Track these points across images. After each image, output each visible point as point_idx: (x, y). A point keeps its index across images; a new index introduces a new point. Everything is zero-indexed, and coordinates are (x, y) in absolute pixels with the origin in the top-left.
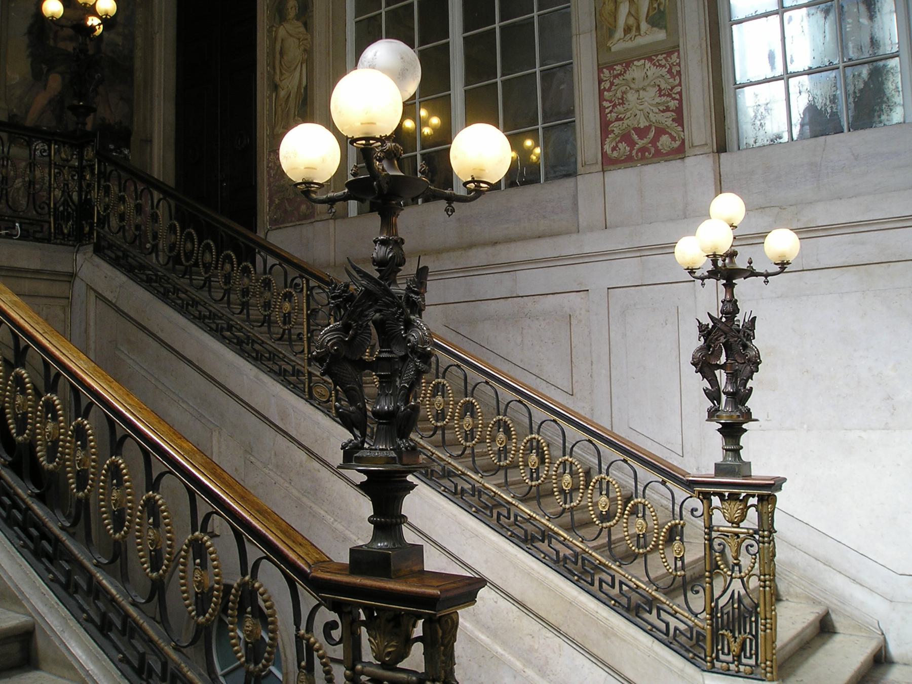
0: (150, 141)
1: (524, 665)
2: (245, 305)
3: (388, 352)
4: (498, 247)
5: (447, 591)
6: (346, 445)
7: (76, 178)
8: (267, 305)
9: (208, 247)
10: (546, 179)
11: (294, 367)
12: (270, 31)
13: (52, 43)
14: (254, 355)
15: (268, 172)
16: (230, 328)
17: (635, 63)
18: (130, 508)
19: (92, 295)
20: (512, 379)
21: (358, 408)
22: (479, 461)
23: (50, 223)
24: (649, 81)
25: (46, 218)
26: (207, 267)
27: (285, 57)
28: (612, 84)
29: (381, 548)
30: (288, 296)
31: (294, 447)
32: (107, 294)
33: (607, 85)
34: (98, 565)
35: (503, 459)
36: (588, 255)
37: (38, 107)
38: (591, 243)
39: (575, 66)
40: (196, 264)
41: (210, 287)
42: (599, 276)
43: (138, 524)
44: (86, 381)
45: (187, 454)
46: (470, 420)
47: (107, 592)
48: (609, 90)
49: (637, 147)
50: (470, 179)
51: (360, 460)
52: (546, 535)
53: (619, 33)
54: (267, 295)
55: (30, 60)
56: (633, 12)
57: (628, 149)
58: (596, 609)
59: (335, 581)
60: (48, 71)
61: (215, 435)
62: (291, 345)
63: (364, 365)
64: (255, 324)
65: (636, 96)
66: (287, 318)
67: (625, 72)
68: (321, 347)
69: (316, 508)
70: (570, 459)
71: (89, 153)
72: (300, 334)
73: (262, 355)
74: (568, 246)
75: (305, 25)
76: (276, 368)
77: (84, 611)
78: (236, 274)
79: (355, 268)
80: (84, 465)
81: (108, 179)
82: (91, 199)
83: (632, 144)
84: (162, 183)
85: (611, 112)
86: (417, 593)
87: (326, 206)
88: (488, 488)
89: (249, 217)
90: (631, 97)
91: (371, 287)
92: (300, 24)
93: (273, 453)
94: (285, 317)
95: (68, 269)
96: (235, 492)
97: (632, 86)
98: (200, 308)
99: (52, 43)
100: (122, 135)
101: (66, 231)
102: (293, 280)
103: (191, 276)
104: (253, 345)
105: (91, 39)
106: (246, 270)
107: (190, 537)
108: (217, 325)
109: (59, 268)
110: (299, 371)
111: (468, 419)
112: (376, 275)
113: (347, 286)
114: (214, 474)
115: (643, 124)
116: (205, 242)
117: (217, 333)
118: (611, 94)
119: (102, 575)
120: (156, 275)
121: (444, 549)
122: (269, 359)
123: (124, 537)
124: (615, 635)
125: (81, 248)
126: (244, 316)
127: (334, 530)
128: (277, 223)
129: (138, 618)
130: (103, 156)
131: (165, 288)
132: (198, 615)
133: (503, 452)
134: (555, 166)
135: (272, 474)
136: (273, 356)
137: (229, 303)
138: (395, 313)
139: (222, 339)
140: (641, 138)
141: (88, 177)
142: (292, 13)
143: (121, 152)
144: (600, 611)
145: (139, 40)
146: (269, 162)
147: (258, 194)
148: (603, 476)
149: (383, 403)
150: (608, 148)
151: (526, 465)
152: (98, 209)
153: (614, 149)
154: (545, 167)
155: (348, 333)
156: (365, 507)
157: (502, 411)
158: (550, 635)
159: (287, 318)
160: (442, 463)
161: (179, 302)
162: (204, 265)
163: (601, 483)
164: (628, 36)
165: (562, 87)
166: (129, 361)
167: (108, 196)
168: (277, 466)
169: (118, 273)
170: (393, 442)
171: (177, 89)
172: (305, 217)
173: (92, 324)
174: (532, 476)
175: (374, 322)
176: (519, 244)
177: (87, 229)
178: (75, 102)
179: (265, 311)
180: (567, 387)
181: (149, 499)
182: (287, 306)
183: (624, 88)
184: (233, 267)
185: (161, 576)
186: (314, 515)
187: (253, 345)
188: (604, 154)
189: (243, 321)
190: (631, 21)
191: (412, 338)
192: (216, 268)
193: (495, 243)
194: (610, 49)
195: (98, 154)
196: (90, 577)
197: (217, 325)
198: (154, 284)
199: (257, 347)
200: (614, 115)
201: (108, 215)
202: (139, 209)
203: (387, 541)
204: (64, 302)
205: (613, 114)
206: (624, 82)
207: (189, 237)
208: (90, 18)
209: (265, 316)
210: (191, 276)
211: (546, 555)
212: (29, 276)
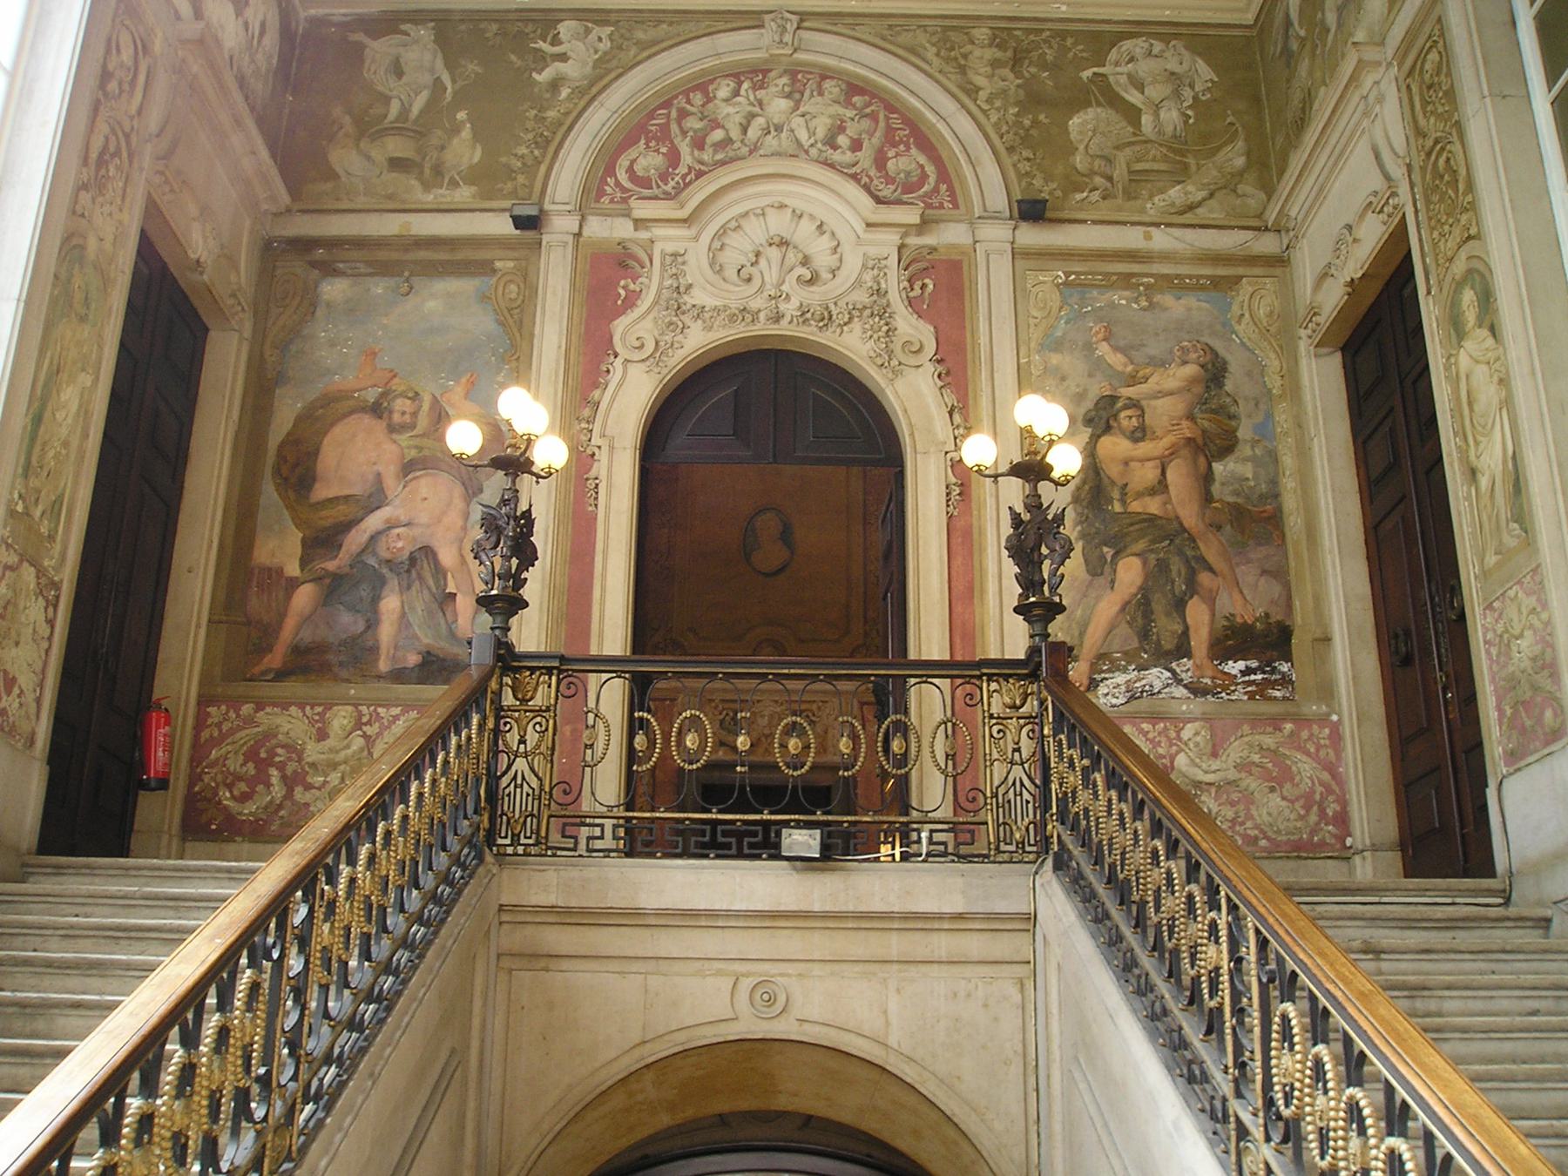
0: (1327, 640)
13: (1118, 507)
15: (1488, 652)
27: (1476, 408)
60: (1116, 554)
99: (1118, 507)
109: (1001, 907)
142: (1470, 316)
145: (1288, 461)
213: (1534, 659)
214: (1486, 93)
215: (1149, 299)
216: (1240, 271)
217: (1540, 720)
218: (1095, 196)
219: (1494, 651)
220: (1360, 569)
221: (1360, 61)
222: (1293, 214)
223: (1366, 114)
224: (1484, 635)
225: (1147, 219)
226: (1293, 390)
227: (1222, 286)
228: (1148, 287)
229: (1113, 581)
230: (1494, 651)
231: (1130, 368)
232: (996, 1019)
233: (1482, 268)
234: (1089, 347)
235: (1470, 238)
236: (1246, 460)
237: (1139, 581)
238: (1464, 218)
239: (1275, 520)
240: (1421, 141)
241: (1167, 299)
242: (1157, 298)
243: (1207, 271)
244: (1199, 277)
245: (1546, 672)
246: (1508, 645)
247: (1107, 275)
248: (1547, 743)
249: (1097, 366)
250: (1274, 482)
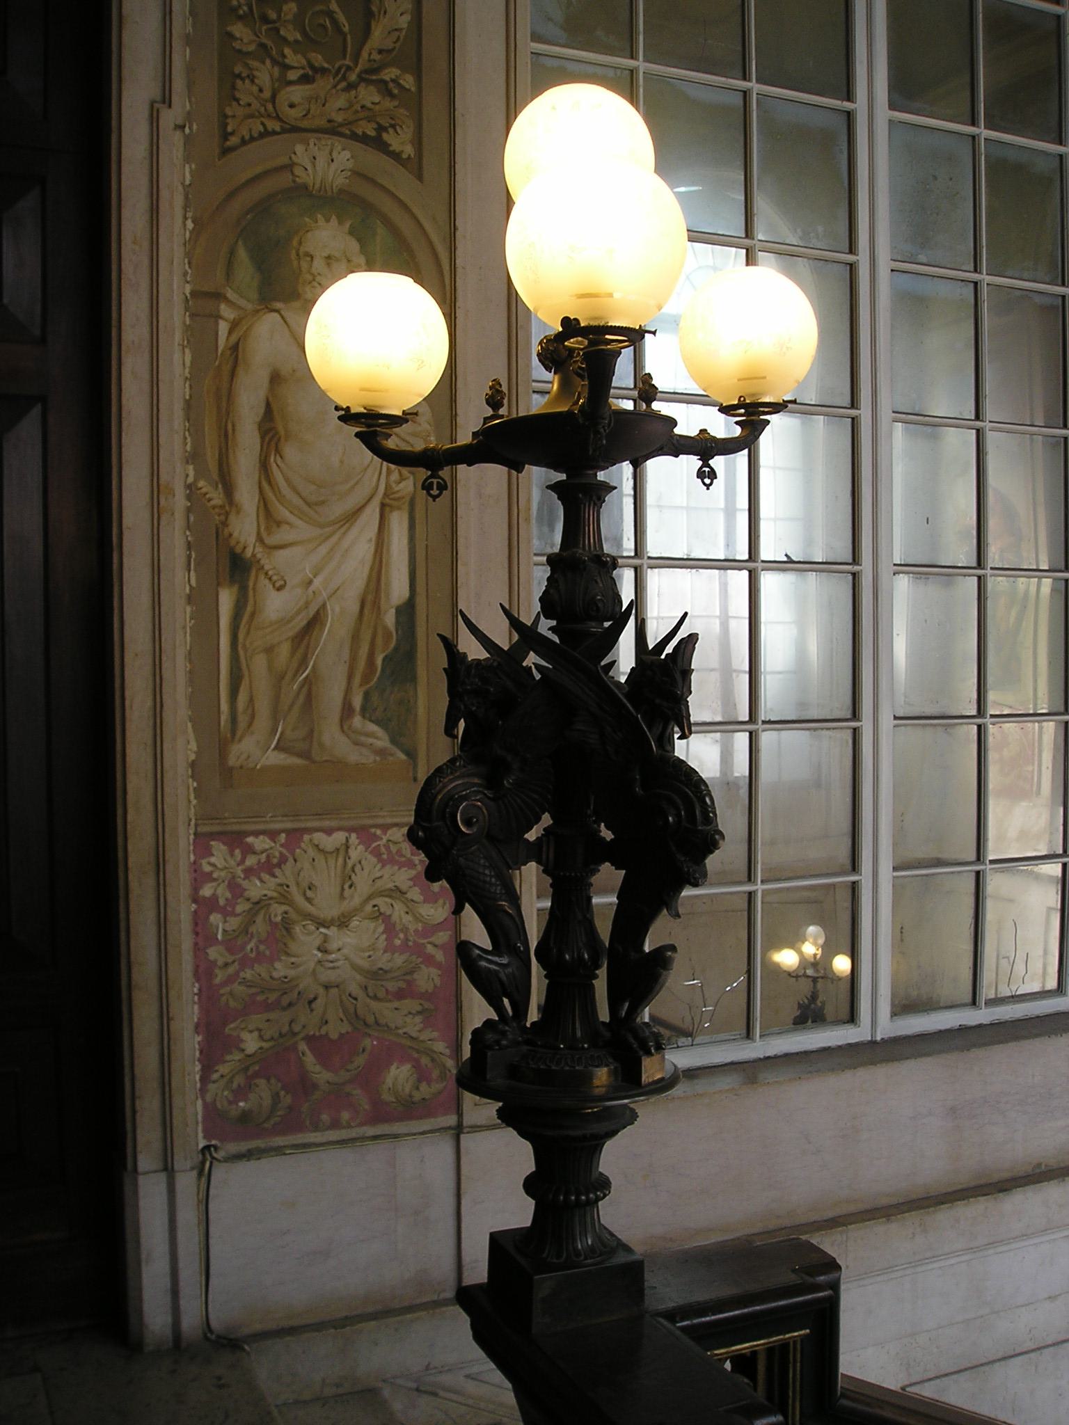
15: (199, 922)
146: (199, 878)
213: (377, 974)
217: (370, 1077)
246: (287, 925)
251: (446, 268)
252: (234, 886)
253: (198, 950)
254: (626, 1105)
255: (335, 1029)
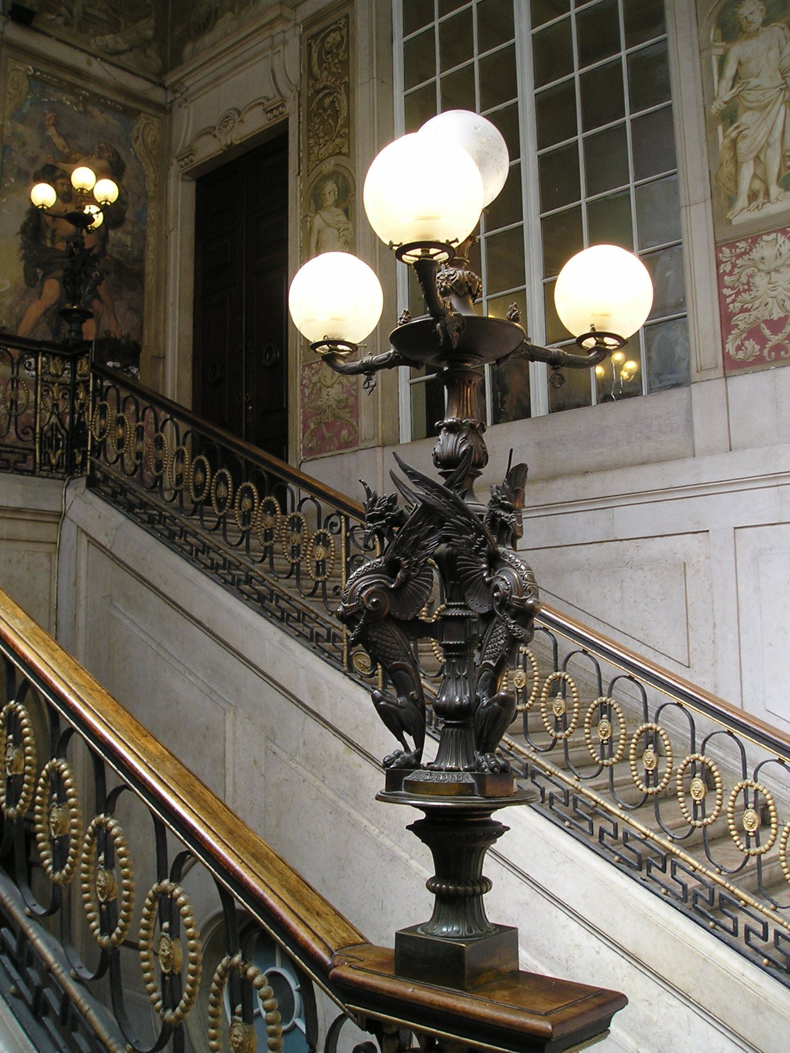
0: (161, 358)
1: (638, 1043)
2: (269, 551)
3: (461, 607)
4: (590, 478)
5: (563, 1022)
6: (392, 760)
7: (67, 397)
8: (295, 552)
9: (222, 477)
10: (650, 391)
11: (329, 630)
12: (304, 221)
13: (49, 244)
14: (279, 614)
15: (302, 391)
16: (249, 580)
17: (765, 238)
18: (75, 837)
19: (84, 539)
20: (620, 647)
21: (411, 699)
22: (574, 754)
23: (35, 451)
24: (784, 259)
25: (30, 445)
26: (221, 504)
28: (734, 266)
29: (446, 936)
30: (322, 540)
31: (328, 734)
32: (101, 538)
33: (728, 268)
34: (32, 916)
35: (700, 815)
36: (707, 486)
37: (32, 319)
38: (711, 469)
39: (685, 246)
40: (208, 502)
41: (225, 530)
42: (721, 512)
43: (85, 861)
44: (18, 649)
45: (154, 762)
46: (562, 702)
47: (43, 958)
48: (731, 274)
49: (770, 344)
50: (588, 331)
51: (414, 787)
52: (666, 859)
53: (742, 201)
54: (296, 537)
55: (23, 263)
56: (759, 173)
57: (757, 347)
58: (741, 970)
59: (372, 987)
60: (44, 276)
61: (230, 716)
62: (325, 602)
63: (424, 630)
64: (280, 575)
65: (766, 279)
66: (320, 567)
67: (751, 250)
68: (351, 598)
69: (355, 814)
70: (702, 758)
71: (84, 366)
72: (336, 588)
73: (289, 615)
74: (680, 474)
75: (346, 212)
76: (307, 631)
77: (13, 982)
78: (258, 513)
79: (405, 468)
80: (16, 769)
81: (104, 398)
82: (84, 423)
83: (762, 341)
84: (176, 404)
85: (733, 301)
86: (510, 1024)
87: (363, 377)
88: (588, 796)
89: (279, 443)
90: (760, 281)
91: (433, 500)
92: (340, 211)
93: (302, 740)
94: (318, 566)
95: (58, 509)
96: (222, 823)
97: (761, 267)
98: (212, 555)
99: (49, 244)
100: (131, 352)
101: (54, 461)
102: (329, 518)
103: (202, 516)
104: (277, 602)
105: (88, 232)
106: (269, 507)
107: (155, 886)
108: (233, 576)
109: (45, 506)
110: (335, 635)
111: (559, 701)
112: (441, 481)
113: (393, 499)
114: (191, 793)
115: (777, 314)
116: (219, 471)
117: (233, 585)
118: (733, 278)
119: (36, 930)
120: (160, 515)
121: (526, 876)
122: (298, 621)
123: (65, 879)
124: (771, 1009)
125: (72, 482)
126: (266, 564)
127: (380, 845)
128: (312, 453)
129: (82, 1002)
130: (99, 371)
131: (170, 530)
132: (165, 1007)
133: (651, 777)
134: (661, 374)
135: (300, 768)
136: (303, 616)
137: (248, 548)
138: (470, 544)
139: (240, 594)
140: (775, 333)
141: (81, 396)
142: (330, 199)
143: (128, 371)
144: (747, 973)
145: (151, 240)
146: (303, 378)
147: (290, 419)
148: (749, 782)
149: (452, 690)
150: (730, 347)
151: (688, 793)
152: (92, 434)
153: (739, 348)
154: (649, 375)
155: (394, 576)
156: (421, 862)
157: (605, 692)
158: (675, 1002)
159: (320, 567)
160: (521, 757)
161: (188, 548)
162: (218, 500)
163: (746, 791)
164: (754, 204)
165: (668, 274)
166: (126, 622)
167: (105, 418)
168: (307, 759)
169: (114, 512)
170: (469, 758)
171: (195, 298)
172: (347, 445)
173: (83, 574)
174: (695, 811)
175: (437, 558)
176: (617, 473)
177: (79, 459)
178: (68, 306)
179: (293, 558)
180: (682, 656)
181: (100, 826)
182: (321, 551)
183: (749, 271)
184: (253, 503)
185: (113, 942)
186: (354, 824)
187: (277, 602)
188: (725, 355)
189: (266, 572)
190: (758, 185)
191: (501, 584)
192: (232, 507)
193: (585, 473)
194: (730, 221)
195: (93, 366)
196: (23, 937)
197: (233, 576)
198: (157, 526)
199: (283, 604)
200: (738, 305)
201: (105, 441)
202: (140, 433)
203: (457, 921)
204: (51, 548)
205: (736, 304)
206: (750, 263)
207: (200, 465)
208: (87, 207)
209: (293, 564)
210: (202, 516)
211: (668, 890)
212: (8, 515)
213: (339, 401)
214: (375, 76)
215: (84, 106)
216: (140, 107)
217: (337, 435)
218: (60, 21)
219: (307, 391)
220: (189, 318)
221: (281, 14)
222: (187, 84)
223: (272, 47)
224: (302, 380)
225: (90, 50)
226: (162, 195)
227: (128, 113)
228: (84, 97)
229: (41, 293)
230: (307, 391)
231: (67, 150)
232: (34, 578)
233: (346, 173)
234: (43, 128)
235: (340, 153)
236: (128, 233)
237: (56, 297)
238: (338, 141)
239: (140, 276)
240: (312, 82)
241: (96, 111)
242: (90, 108)
243: (121, 100)
244: (116, 103)
245: (348, 410)
246: (320, 390)
247: (61, 80)
248: (339, 448)
249: (47, 142)
250: (142, 252)
251: (323, 35)
252: (310, 380)
253: (302, 400)
254: (234, 453)
255: (331, 420)
